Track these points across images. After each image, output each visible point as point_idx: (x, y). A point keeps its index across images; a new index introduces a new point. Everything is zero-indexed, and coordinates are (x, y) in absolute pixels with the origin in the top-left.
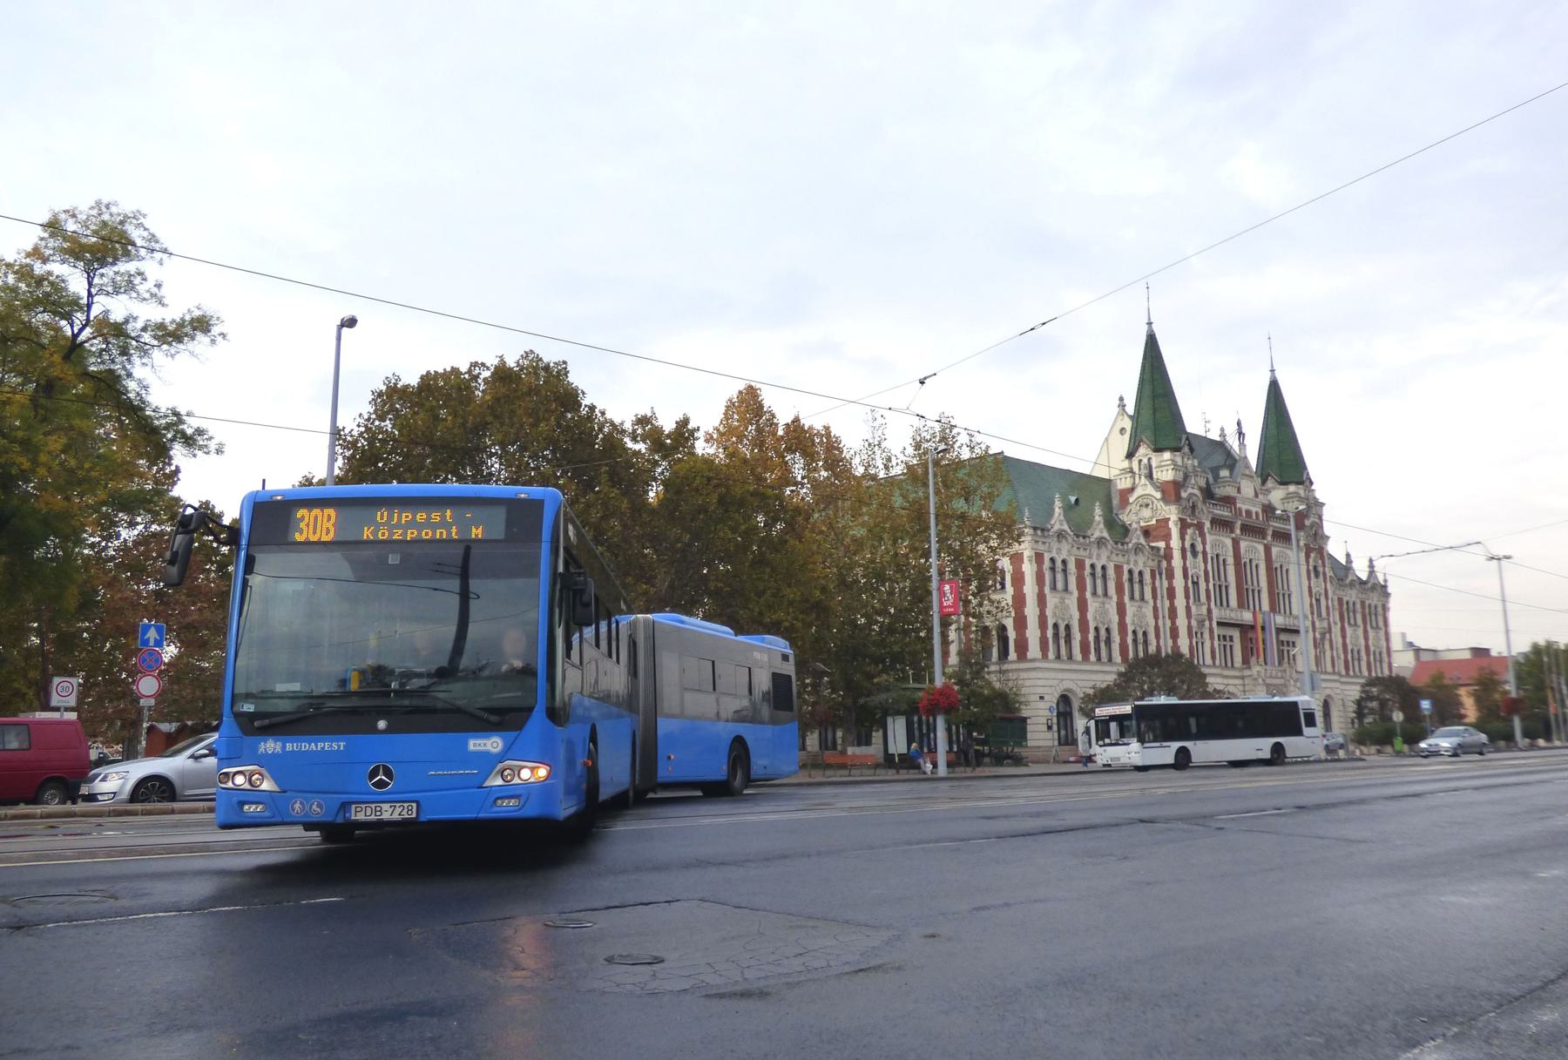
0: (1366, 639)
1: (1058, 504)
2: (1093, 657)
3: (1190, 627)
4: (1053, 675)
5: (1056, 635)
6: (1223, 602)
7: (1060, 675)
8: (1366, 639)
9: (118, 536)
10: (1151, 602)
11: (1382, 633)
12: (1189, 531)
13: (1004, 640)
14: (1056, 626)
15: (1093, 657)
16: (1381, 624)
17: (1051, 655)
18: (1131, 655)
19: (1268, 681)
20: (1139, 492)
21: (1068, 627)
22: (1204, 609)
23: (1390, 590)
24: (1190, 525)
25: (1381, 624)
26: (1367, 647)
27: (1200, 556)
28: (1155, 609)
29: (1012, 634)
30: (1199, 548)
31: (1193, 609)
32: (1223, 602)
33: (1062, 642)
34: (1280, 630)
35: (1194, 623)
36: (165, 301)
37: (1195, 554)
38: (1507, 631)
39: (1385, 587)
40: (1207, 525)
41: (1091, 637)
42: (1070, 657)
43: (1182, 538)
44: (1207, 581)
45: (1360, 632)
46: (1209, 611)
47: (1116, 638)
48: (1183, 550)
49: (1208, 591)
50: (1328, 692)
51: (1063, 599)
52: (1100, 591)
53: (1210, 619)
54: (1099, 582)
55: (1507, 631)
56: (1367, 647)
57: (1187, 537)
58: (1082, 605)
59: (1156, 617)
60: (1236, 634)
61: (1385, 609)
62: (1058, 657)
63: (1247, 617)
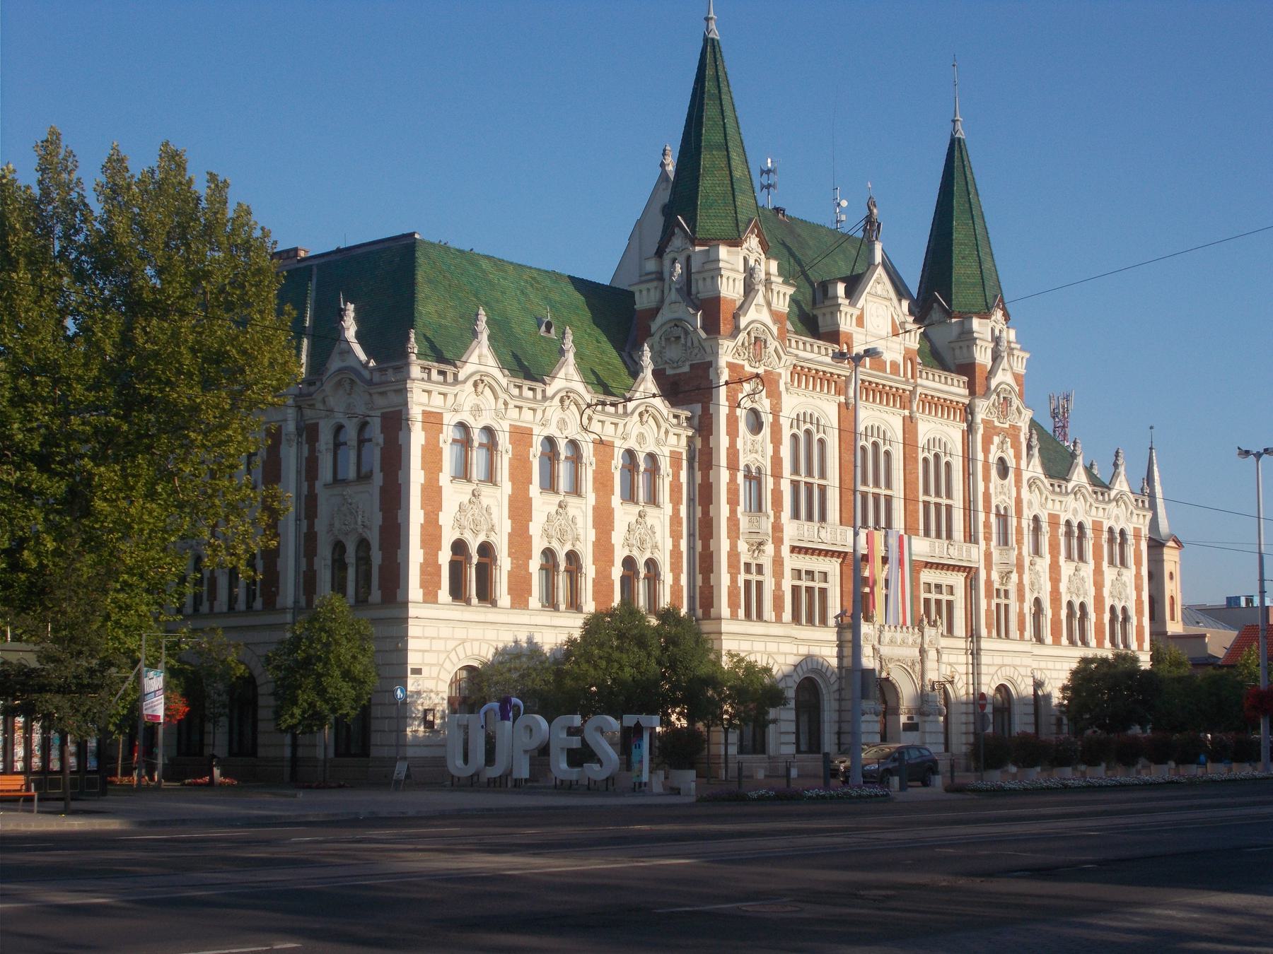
1: (483, 318)
2: (1064, 640)
4: (445, 631)
7: (460, 633)
8: (1099, 585)
13: (364, 559)
15: (535, 601)
20: (665, 315)
22: (767, 525)
26: (1099, 599)
29: (376, 557)
36: (208, 177)
37: (756, 426)
38: (1262, 580)
40: (785, 376)
43: (986, 451)
47: (1092, 616)
50: (1009, 672)
53: (778, 542)
55: (1262, 580)
56: (1099, 599)
57: (993, 448)
59: (676, 536)
60: (832, 567)
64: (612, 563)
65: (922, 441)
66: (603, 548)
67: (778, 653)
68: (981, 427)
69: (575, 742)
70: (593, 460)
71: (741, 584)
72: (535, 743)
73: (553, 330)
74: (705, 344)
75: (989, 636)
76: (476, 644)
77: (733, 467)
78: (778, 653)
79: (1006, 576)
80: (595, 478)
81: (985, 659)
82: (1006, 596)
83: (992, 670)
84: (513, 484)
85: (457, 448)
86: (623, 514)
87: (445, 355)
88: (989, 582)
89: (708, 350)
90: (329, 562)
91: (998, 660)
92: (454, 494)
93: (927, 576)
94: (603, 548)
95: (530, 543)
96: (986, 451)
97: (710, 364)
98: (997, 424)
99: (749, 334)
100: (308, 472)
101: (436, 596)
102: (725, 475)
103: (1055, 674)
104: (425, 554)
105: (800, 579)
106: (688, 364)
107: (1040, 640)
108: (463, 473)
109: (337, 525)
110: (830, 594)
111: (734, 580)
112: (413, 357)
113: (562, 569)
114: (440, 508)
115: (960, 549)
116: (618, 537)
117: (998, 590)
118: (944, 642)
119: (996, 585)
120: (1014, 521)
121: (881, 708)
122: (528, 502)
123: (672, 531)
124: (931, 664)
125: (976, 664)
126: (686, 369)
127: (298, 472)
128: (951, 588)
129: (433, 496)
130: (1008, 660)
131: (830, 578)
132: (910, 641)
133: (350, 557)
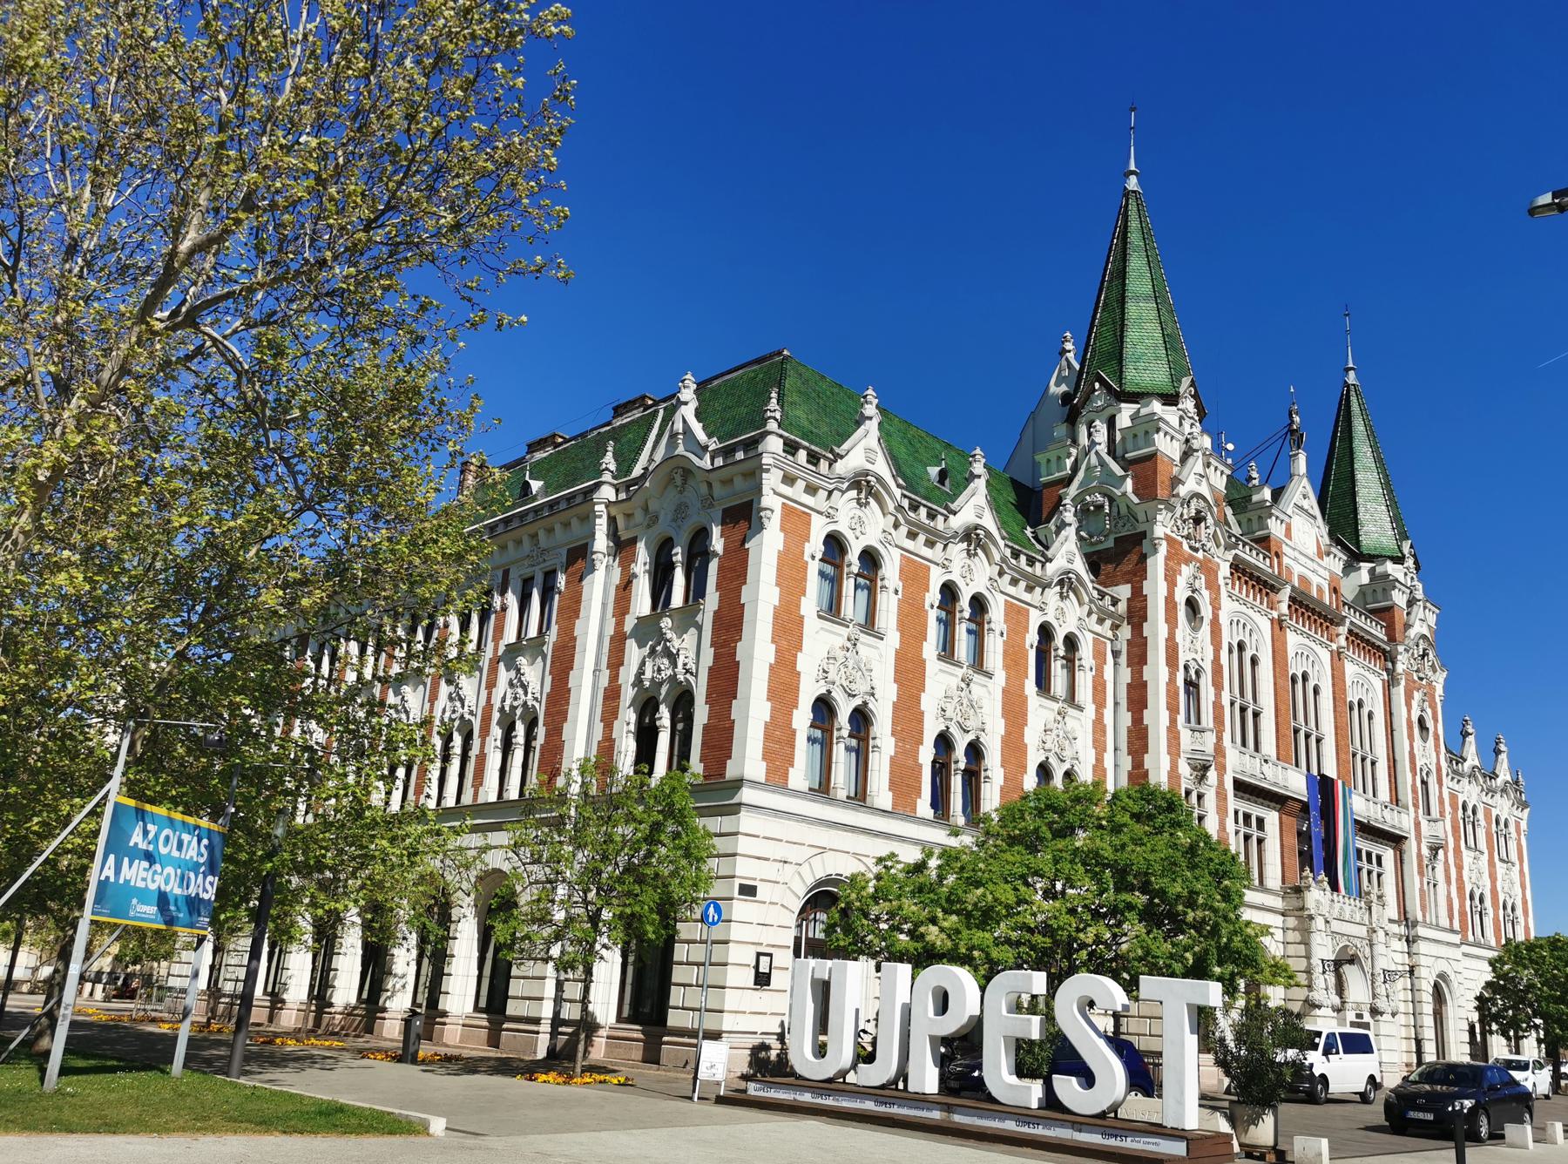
2: (924, 807)
5: (941, 769)
6: (1249, 739)
9: (939, 857)
10: (1090, 710)
12: (1186, 571)
14: (944, 742)
21: (975, 751)
22: (1210, 739)
27: (1206, 628)
28: (1099, 724)
30: (1206, 611)
31: (1185, 735)
32: (1249, 739)
33: (957, 783)
34: (1242, 788)
40: (1225, 570)
41: (926, 754)
42: (860, 797)
44: (1218, 686)
46: (1219, 750)
48: (1170, 602)
49: (1218, 706)
50: (1442, 966)
51: (967, 682)
58: (1015, 712)
59: (1099, 746)
62: (823, 789)
64: (1024, 768)
66: (1014, 746)
69: (1034, 1028)
70: (1004, 627)
72: (951, 1024)
73: (947, 482)
74: (1136, 509)
77: (1172, 660)
80: (1005, 652)
82: (1379, 864)
84: (902, 636)
85: (827, 586)
86: (1039, 712)
87: (821, 440)
89: (1141, 517)
90: (632, 727)
92: (820, 642)
94: (1014, 746)
95: (921, 721)
97: (1143, 535)
100: (618, 600)
101: (786, 776)
102: (1164, 672)
103: (1468, 984)
104: (773, 709)
106: (1112, 538)
108: (832, 609)
109: (648, 674)
112: (772, 426)
113: (954, 768)
114: (799, 647)
116: (1032, 735)
119: (1426, 862)
121: (1337, 1000)
122: (1023, 700)
123: (1095, 741)
126: (1110, 543)
127: (604, 605)
129: (788, 630)
131: (1267, 827)
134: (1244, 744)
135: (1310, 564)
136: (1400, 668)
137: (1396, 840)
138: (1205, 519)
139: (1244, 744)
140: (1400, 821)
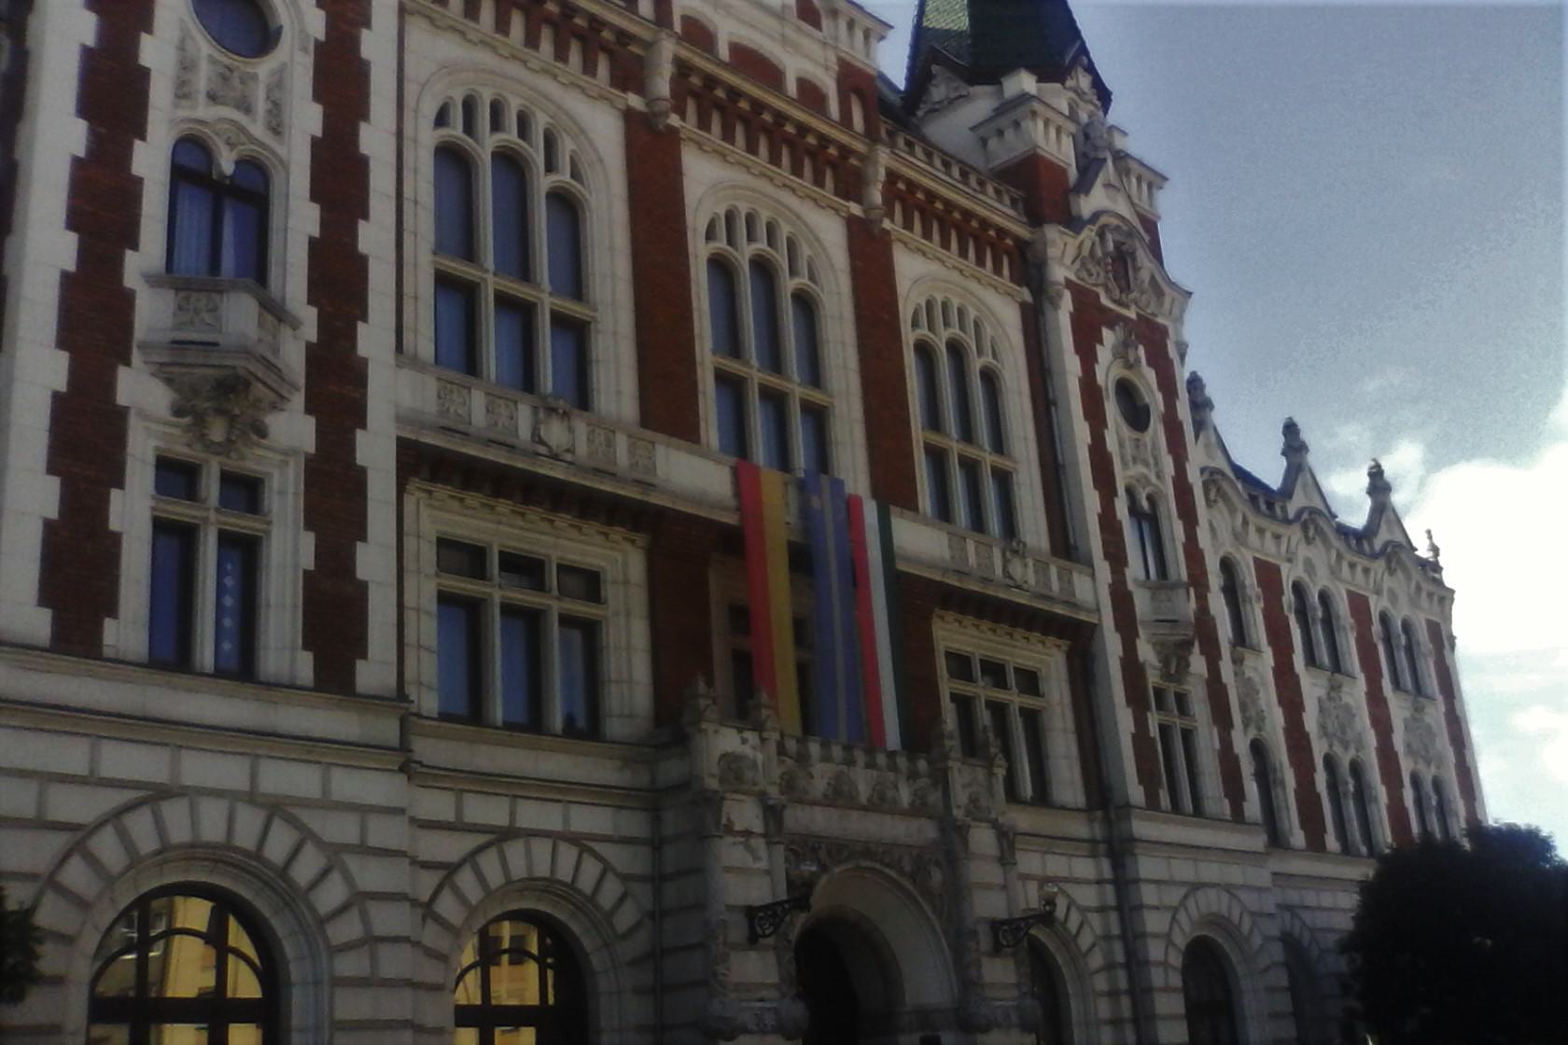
0: (1382, 724)
3: (1132, 667)
11: (1435, 714)
15: (127, 630)
16: (1432, 684)
17: (127, 630)
18: (1415, 828)
19: (802, 819)
23: (1449, 579)
24: (1113, 320)
25: (1432, 684)
27: (1157, 429)
35: (1146, 652)
37: (1137, 416)
39: (1436, 568)
41: (1321, 779)
43: (1088, 359)
45: (1356, 692)
50: (1213, 902)
52: (1324, 655)
54: (1319, 633)
57: (1104, 354)
60: (622, 563)
61: (1442, 640)
62: (171, 654)
63: (694, 475)
65: (907, 306)
67: (326, 804)
68: (1067, 296)
71: (1154, 731)
75: (1152, 802)
76: (542, 849)
78: (326, 804)
79: (1174, 657)
81: (1147, 866)
83: (1174, 896)
88: (1132, 667)
91: (1184, 870)
93: (950, 634)
96: (1088, 359)
98: (1105, 301)
99: (1101, 235)
105: (969, 678)
107: (242, 667)
110: (613, 636)
111: (1140, 723)
115: (1042, 568)
117: (1159, 693)
118: (1023, 820)
119: (1153, 678)
120: (1178, 529)
124: (983, 870)
125: (1123, 882)
128: (590, 584)
130: (1210, 871)
131: (610, 591)
132: (905, 795)
133: (1247, 767)
134: (978, 524)
135: (772, 23)
136: (1060, 272)
137: (1077, 637)
138: (1133, 254)
139: (978, 524)
140: (1090, 590)
